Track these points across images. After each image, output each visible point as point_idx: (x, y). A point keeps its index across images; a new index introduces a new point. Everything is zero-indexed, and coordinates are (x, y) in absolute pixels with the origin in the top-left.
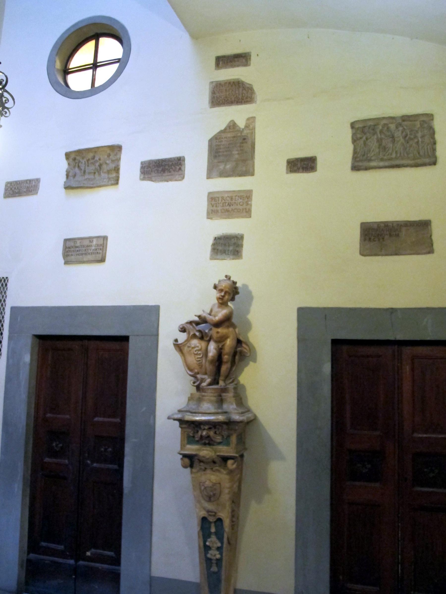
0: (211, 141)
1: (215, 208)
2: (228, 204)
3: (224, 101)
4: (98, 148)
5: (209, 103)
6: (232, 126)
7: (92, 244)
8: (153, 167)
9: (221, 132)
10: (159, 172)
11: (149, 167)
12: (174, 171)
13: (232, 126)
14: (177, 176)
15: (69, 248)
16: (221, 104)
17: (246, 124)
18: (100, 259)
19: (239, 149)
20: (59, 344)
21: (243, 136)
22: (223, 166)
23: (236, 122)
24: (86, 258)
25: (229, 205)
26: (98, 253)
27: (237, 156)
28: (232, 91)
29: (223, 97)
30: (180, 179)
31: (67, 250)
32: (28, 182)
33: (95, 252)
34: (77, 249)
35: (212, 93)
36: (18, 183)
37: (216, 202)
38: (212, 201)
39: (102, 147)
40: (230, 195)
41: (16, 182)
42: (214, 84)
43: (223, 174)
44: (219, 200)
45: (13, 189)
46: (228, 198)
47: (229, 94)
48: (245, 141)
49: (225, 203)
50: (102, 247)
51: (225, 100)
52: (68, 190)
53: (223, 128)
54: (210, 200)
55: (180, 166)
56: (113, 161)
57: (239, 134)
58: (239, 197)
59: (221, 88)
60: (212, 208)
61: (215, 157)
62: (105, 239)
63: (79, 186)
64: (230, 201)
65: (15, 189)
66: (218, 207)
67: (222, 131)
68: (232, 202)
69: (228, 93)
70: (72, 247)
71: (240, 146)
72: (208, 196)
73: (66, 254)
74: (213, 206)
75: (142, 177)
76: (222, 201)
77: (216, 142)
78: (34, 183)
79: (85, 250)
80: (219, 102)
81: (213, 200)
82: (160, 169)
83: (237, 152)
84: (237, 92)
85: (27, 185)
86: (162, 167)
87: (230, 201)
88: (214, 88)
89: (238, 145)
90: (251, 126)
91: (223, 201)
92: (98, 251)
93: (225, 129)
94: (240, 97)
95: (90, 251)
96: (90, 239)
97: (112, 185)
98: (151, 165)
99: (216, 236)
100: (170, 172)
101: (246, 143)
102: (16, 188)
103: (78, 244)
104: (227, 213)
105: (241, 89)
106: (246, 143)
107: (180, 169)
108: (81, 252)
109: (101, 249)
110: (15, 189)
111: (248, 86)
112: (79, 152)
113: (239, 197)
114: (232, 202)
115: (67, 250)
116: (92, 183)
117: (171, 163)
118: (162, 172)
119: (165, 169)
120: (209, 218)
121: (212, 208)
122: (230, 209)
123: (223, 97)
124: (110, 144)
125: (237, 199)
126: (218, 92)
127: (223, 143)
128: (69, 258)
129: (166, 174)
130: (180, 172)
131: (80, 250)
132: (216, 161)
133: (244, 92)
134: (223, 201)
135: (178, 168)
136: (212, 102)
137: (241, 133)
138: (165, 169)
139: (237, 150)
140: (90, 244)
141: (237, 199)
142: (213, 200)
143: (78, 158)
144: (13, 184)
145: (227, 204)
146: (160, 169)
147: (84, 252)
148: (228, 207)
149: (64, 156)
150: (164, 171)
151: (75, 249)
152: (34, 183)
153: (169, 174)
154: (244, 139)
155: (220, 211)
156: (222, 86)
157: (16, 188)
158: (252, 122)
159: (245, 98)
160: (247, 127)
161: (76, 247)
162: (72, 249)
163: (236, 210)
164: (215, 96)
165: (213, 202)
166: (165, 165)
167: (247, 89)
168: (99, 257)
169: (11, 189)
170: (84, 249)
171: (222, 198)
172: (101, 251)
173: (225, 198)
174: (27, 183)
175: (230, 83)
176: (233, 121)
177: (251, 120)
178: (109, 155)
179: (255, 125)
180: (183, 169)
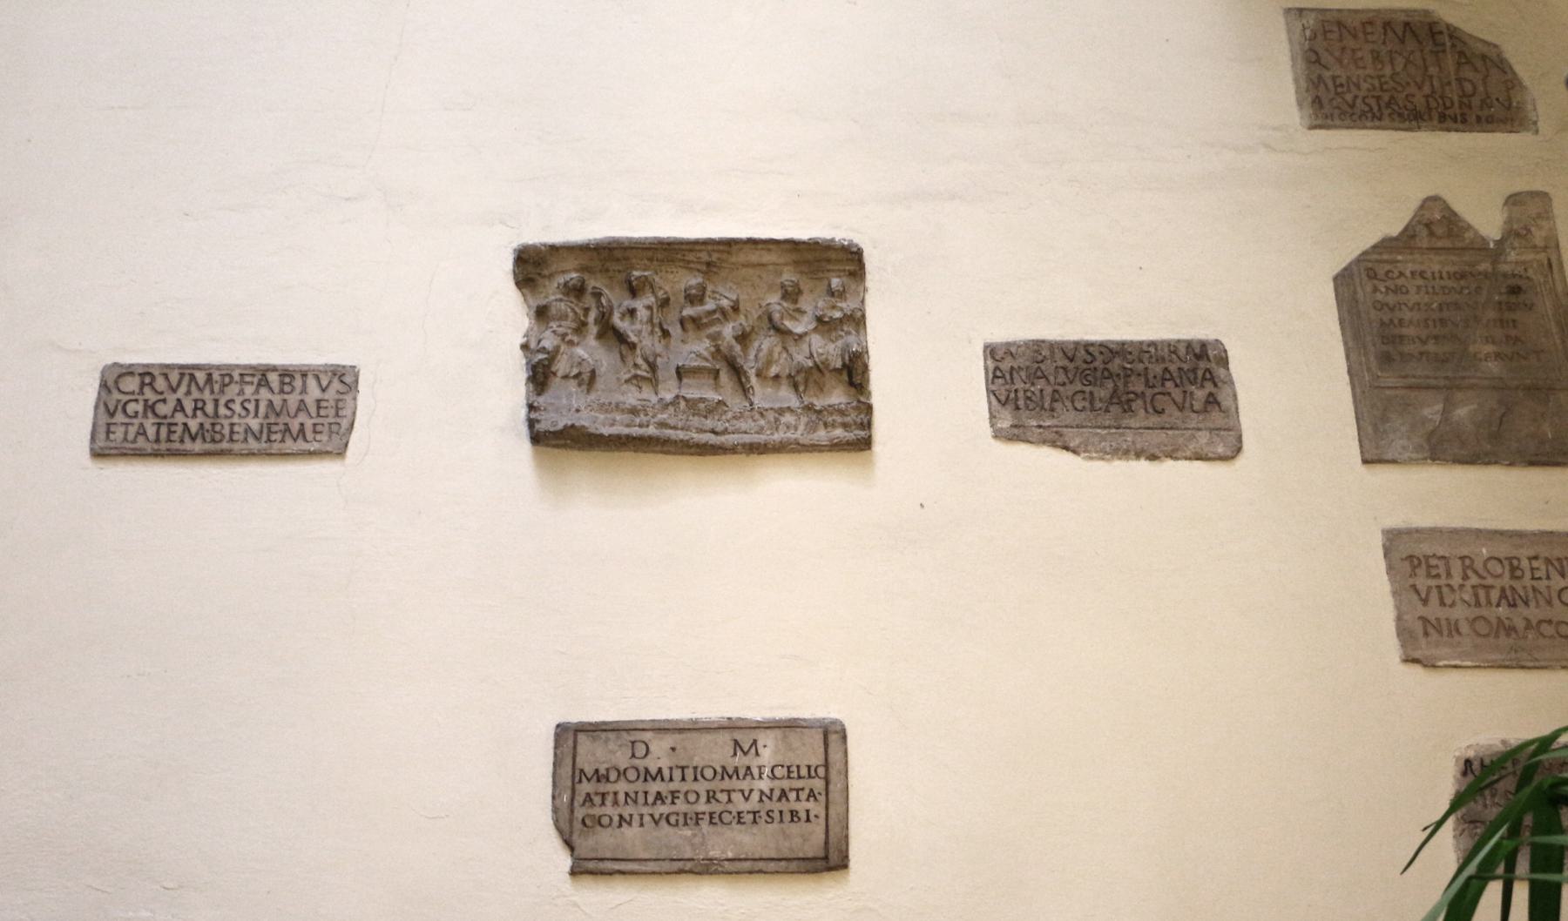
0: (1343, 280)
1: (1433, 611)
2: (1503, 595)
3: (1373, 102)
4: (729, 244)
5: (1300, 104)
6: (1436, 225)
7: (754, 763)
8: (1062, 378)
9: (1386, 245)
10: (1098, 405)
11: (1036, 375)
12: (1181, 409)
13: (1436, 225)
14: (1203, 437)
15: (599, 777)
16: (1363, 115)
17: (1509, 221)
18: (814, 846)
19: (1498, 333)
20: (1544, 459)
21: (1505, 275)
22: (1439, 407)
23: (1458, 207)
24: (722, 843)
25: (1510, 599)
26: (794, 813)
27: (1493, 367)
28: (1408, 61)
29: (1365, 86)
30: (1220, 450)
31: (586, 787)
32: (273, 378)
33: (780, 807)
34: (654, 787)
35: (1309, 62)
36: (201, 377)
37: (1433, 582)
38: (1413, 574)
39: (753, 242)
40: (1503, 550)
41: (188, 372)
42: (1311, 20)
43: (1443, 448)
44: (1449, 575)
45: (163, 409)
46: (1496, 568)
47: (1394, 75)
48: (1522, 298)
49: (1488, 588)
50: (818, 784)
51: (1378, 98)
52: (541, 449)
53: (1395, 230)
54: (1407, 566)
55: (1209, 387)
56: (824, 324)
57: (1485, 266)
58: (1548, 561)
59: (1350, 43)
60: (1422, 610)
61: (1386, 359)
62: (833, 738)
63: (636, 431)
64: (1506, 581)
65: (180, 406)
66: (1453, 605)
67: (1392, 239)
68: (1517, 585)
69: (1388, 71)
70: (622, 774)
71: (1502, 323)
72: (1387, 552)
73: (580, 813)
74: (1425, 602)
75: (1005, 423)
76: (1465, 577)
77: (1375, 290)
78: (314, 392)
79: (711, 796)
80: (1352, 106)
81: (1422, 571)
82: (1102, 393)
83: (1490, 348)
84: (1433, 70)
85: (264, 394)
86: (1110, 385)
87: (1506, 581)
88: (1314, 37)
89: (1491, 314)
90: (1538, 237)
91: (1474, 580)
92: (801, 807)
93: (1409, 234)
94: (1453, 94)
95: (739, 804)
96: (742, 734)
97: (837, 446)
98: (1048, 367)
99: (1471, 754)
100: (1160, 412)
101: (1530, 307)
102: (189, 406)
103: (660, 755)
104: (1504, 641)
105: (1450, 61)
106: (1530, 307)
107: (1212, 401)
108: (680, 806)
109: (812, 794)
110: (180, 406)
111: (1480, 48)
112: (612, 258)
113: (1548, 561)
114: (1517, 585)
115: (586, 787)
116: (709, 423)
117: (1157, 369)
118: (1115, 409)
119: (1117, 393)
120: (1415, 661)
121: (1422, 610)
122: (1520, 624)
123: (1365, 86)
124: (802, 234)
125: (1541, 573)
126: (1340, 61)
127: (1413, 298)
128: (603, 841)
129: (1140, 418)
130: (1216, 418)
131: (674, 794)
132: (1390, 380)
133: (1468, 73)
134: (1474, 580)
135: (1200, 394)
136: (1317, 102)
137: (1495, 262)
138: (1117, 393)
139: (1489, 340)
140: (740, 761)
141: (1541, 573)
142: (1422, 571)
143: (592, 283)
144: (160, 384)
145: (1495, 595)
146: (1102, 393)
147: (702, 807)
148: (1503, 611)
149: (509, 264)
150: (1123, 402)
151: (639, 786)
152: (314, 392)
153: (1154, 420)
154: (1515, 290)
155: (1465, 628)
156: (1355, 37)
157: (189, 406)
158: (1539, 216)
159: (1476, 101)
160: (1515, 233)
161: (647, 776)
162: (622, 787)
163: (1548, 630)
164: (1327, 74)
165: (1422, 582)
166: (1128, 374)
167: (1479, 64)
168: (811, 839)
169: (150, 408)
170: (702, 787)
171: (1467, 562)
172: (816, 808)
173: (1479, 565)
174: (264, 382)
175: (1387, 25)
176: (1433, 201)
177: (1529, 210)
178: (791, 294)
179: (1553, 229)
180: (1223, 397)
